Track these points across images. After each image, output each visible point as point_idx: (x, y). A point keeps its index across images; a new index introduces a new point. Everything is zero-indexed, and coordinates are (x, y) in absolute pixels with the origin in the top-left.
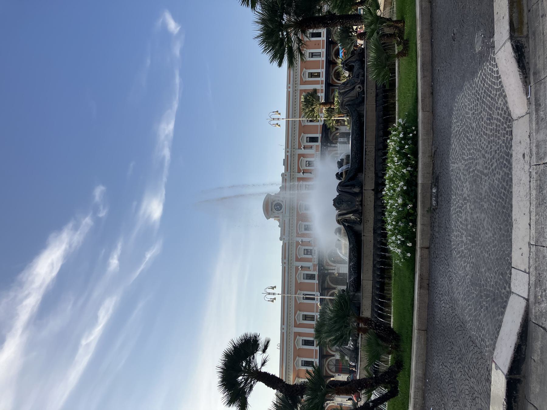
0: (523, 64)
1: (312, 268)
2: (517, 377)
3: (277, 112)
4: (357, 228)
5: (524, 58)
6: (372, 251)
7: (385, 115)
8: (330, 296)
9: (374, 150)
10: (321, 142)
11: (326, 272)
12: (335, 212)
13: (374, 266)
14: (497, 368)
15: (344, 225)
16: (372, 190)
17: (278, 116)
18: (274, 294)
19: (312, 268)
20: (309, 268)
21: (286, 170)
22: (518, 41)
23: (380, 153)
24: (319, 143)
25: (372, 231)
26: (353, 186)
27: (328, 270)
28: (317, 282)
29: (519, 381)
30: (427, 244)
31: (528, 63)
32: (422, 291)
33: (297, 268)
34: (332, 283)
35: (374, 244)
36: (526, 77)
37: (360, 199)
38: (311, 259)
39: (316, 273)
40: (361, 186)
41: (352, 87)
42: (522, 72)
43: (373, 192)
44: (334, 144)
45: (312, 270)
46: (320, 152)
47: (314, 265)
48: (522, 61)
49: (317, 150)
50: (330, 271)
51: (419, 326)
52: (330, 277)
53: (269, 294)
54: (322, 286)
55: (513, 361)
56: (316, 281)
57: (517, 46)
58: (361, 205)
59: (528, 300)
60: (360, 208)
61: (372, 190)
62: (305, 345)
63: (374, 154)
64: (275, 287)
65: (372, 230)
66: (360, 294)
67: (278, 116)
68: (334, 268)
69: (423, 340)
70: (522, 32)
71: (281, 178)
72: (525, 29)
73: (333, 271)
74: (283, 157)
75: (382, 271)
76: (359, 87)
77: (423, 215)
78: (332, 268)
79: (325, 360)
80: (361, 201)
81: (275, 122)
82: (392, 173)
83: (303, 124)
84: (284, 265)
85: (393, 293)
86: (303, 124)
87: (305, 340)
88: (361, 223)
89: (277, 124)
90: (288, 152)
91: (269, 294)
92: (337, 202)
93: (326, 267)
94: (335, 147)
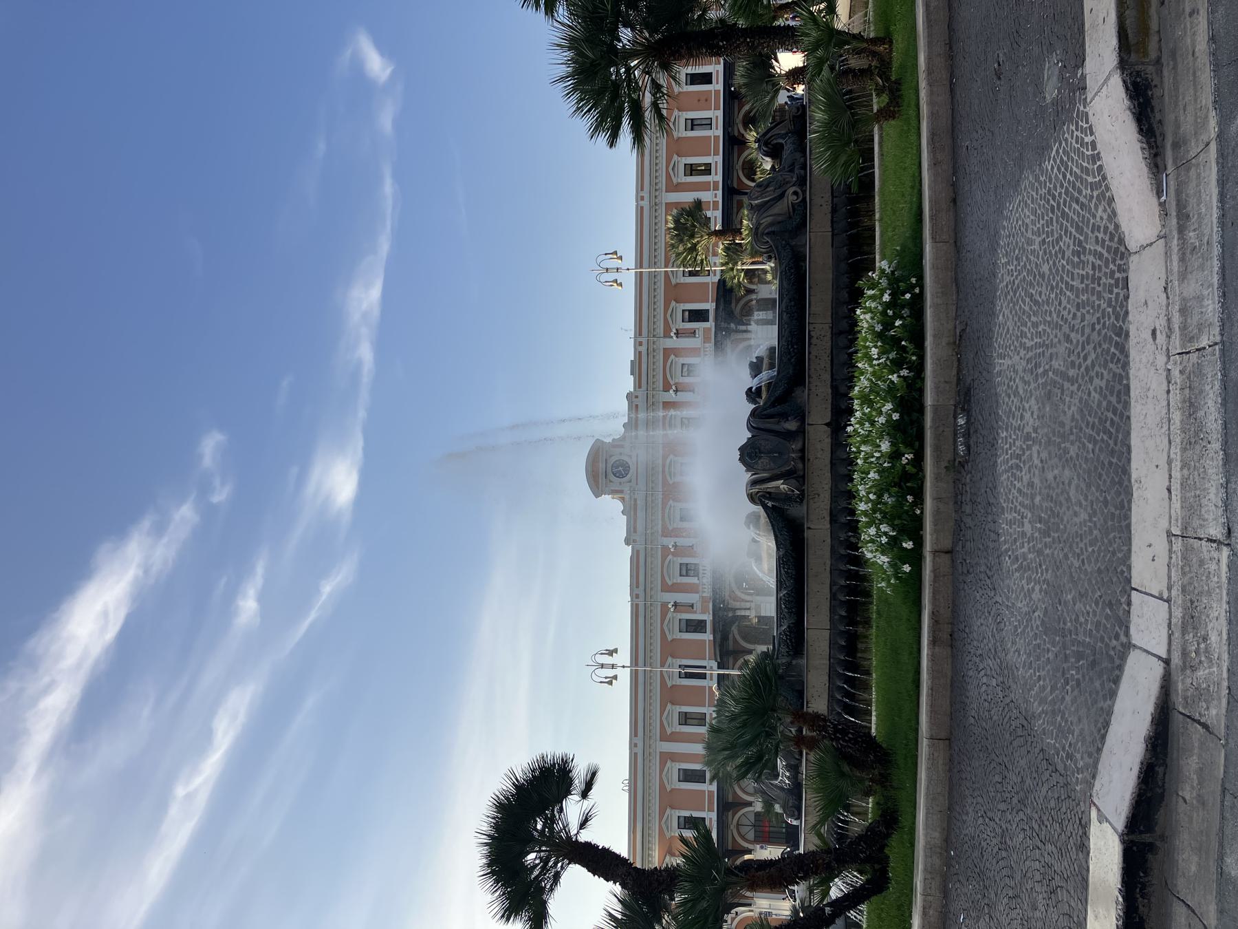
0: (1150, 125)
2: (1147, 838)
3: (615, 253)
4: (795, 511)
5: (1152, 111)
6: (828, 562)
13: (833, 596)
17: (616, 263)
18: (613, 666)
19: (698, 607)
20: (692, 606)
21: (638, 384)
23: (843, 341)
24: (710, 324)
25: (828, 519)
26: (784, 416)
27: (734, 610)
30: (947, 544)
31: (1160, 122)
35: (832, 547)
36: (1156, 155)
37: (799, 445)
39: (708, 617)
40: (801, 416)
41: (779, 192)
42: (1148, 143)
43: (828, 430)
45: (699, 610)
50: (739, 613)
53: (602, 666)
54: (721, 646)
56: (708, 637)
57: (1135, 84)
58: (803, 459)
59: (1167, 662)
60: (800, 466)
64: (616, 651)
68: (748, 605)
69: (941, 762)
70: (1146, 54)
73: (747, 613)
76: (795, 193)
80: (803, 450)
81: (611, 276)
83: (673, 281)
85: (875, 656)
86: (673, 281)
88: (802, 501)
89: (616, 281)
91: (602, 666)
92: (749, 454)
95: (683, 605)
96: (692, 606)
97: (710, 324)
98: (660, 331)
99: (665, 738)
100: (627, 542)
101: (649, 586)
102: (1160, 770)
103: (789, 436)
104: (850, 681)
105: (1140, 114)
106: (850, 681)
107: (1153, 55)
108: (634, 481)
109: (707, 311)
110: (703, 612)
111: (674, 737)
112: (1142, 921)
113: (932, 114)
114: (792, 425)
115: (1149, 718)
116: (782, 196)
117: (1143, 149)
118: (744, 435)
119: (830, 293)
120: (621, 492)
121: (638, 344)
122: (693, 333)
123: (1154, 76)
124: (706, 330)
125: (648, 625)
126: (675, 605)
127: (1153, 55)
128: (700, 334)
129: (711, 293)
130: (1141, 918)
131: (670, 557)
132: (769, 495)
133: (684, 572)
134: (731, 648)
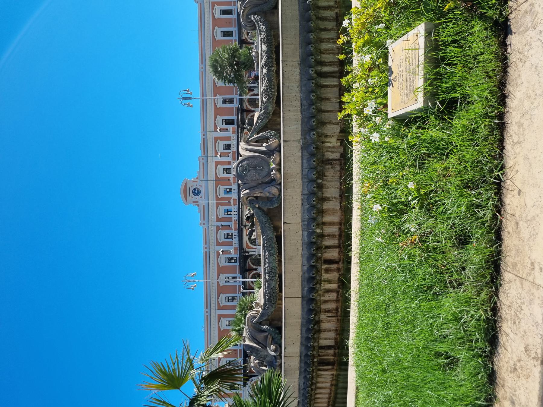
3: (188, 91)
8: (252, 278)
11: (247, 254)
18: (190, 99)
20: (228, 130)
23: (313, 135)
27: (248, 252)
34: (253, 264)
47: (235, 249)
50: (250, 254)
52: (251, 260)
53: (185, 99)
56: (237, 264)
62: (223, 15)
68: (254, 250)
73: (254, 253)
78: (252, 250)
79: (248, 273)
81: (187, 102)
82: (327, 219)
83: (221, 285)
84: (207, 314)
85: (332, 190)
86: (221, 285)
87: (224, 32)
89: (189, 104)
91: (185, 99)
93: (247, 250)
99: (220, 308)
108: (203, 197)
111: (224, 308)
119: (299, 215)
120: (197, 202)
129: (235, 112)
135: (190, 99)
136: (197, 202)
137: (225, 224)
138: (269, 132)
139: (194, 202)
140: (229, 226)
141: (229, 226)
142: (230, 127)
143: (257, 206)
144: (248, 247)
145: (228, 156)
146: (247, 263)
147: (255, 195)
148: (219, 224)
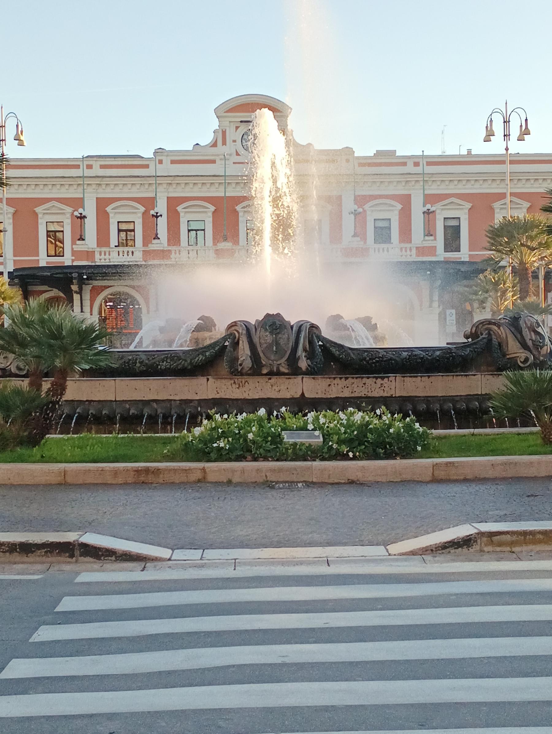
0: (448, 547)
1: (80, 246)
2: (77, 553)
4: (224, 366)
5: (455, 548)
6: (177, 398)
7: (458, 412)
9: (385, 394)
10: (447, 262)
11: (74, 287)
12: (254, 317)
13: (147, 403)
14: (81, 536)
15: (225, 339)
16: (303, 394)
17: (515, 132)
18: (506, 136)
19: (80, 246)
20: (82, 239)
21: (365, 162)
22: (476, 541)
24: (441, 255)
25: (218, 396)
26: (311, 355)
27: (80, 292)
28: (42, 264)
29: (72, 556)
30: (211, 477)
31: (449, 552)
32: (133, 473)
33: (79, 203)
35: (191, 401)
36: (432, 550)
37: (284, 369)
38: (107, 244)
39: (67, 260)
40: (311, 372)
41: (530, 343)
42: (439, 547)
43: (298, 395)
44: (440, 296)
45: (76, 248)
46: (414, 258)
47: (90, 254)
48: (451, 546)
49: (421, 251)
50: (76, 297)
51: (72, 471)
53: (506, 122)
54: (34, 277)
55: (95, 548)
56: (43, 260)
57: (470, 540)
58: (271, 374)
59: (169, 560)
60: (265, 371)
61: (303, 394)
63: (377, 395)
64: (21, 144)
65: (222, 395)
66: (77, 377)
67: (515, 132)
68: (87, 309)
69: (48, 478)
70: (486, 545)
71: (339, 146)
72: (490, 548)
74: (403, 151)
75: (138, 418)
76: (527, 360)
77: (258, 470)
78: (87, 303)
80: (279, 373)
81: (498, 128)
88: (232, 373)
90: (416, 164)
91: (506, 122)
92: (274, 324)
93: (87, 289)
94: (431, 301)
95: (82, 227)
96: (82, 239)
97: (441, 255)
98: (433, 190)
100: (159, 152)
101: (107, 181)
102: (113, 558)
103: (293, 360)
104: (70, 417)
105: (454, 542)
106: (70, 417)
107: (486, 549)
109: (458, 250)
110: (74, 253)
112: (33, 552)
113: (531, 463)
114: (303, 364)
115: (140, 552)
116: (524, 346)
117: (436, 544)
118: (292, 318)
120: (224, 143)
121: (416, 161)
122: (429, 232)
123: (474, 549)
124: (432, 250)
125: (54, 181)
126: (82, 217)
127: (486, 549)
128: (429, 242)
130: (34, 551)
131: (142, 209)
132: (236, 344)
133: (123, 227)
134: (30, 288)
135: (506, 136)
136: (224, 143)
137: (162, 224)
138: (321, 360)
139: (224, 133)
140: (156, 238)
141: (156, 238)
142: (440, 242)
143: (227, 343)
144: (96, 291)
145: (355, 235)
146: (45, 288)
147: (241, 342)
148: (161, 207)
